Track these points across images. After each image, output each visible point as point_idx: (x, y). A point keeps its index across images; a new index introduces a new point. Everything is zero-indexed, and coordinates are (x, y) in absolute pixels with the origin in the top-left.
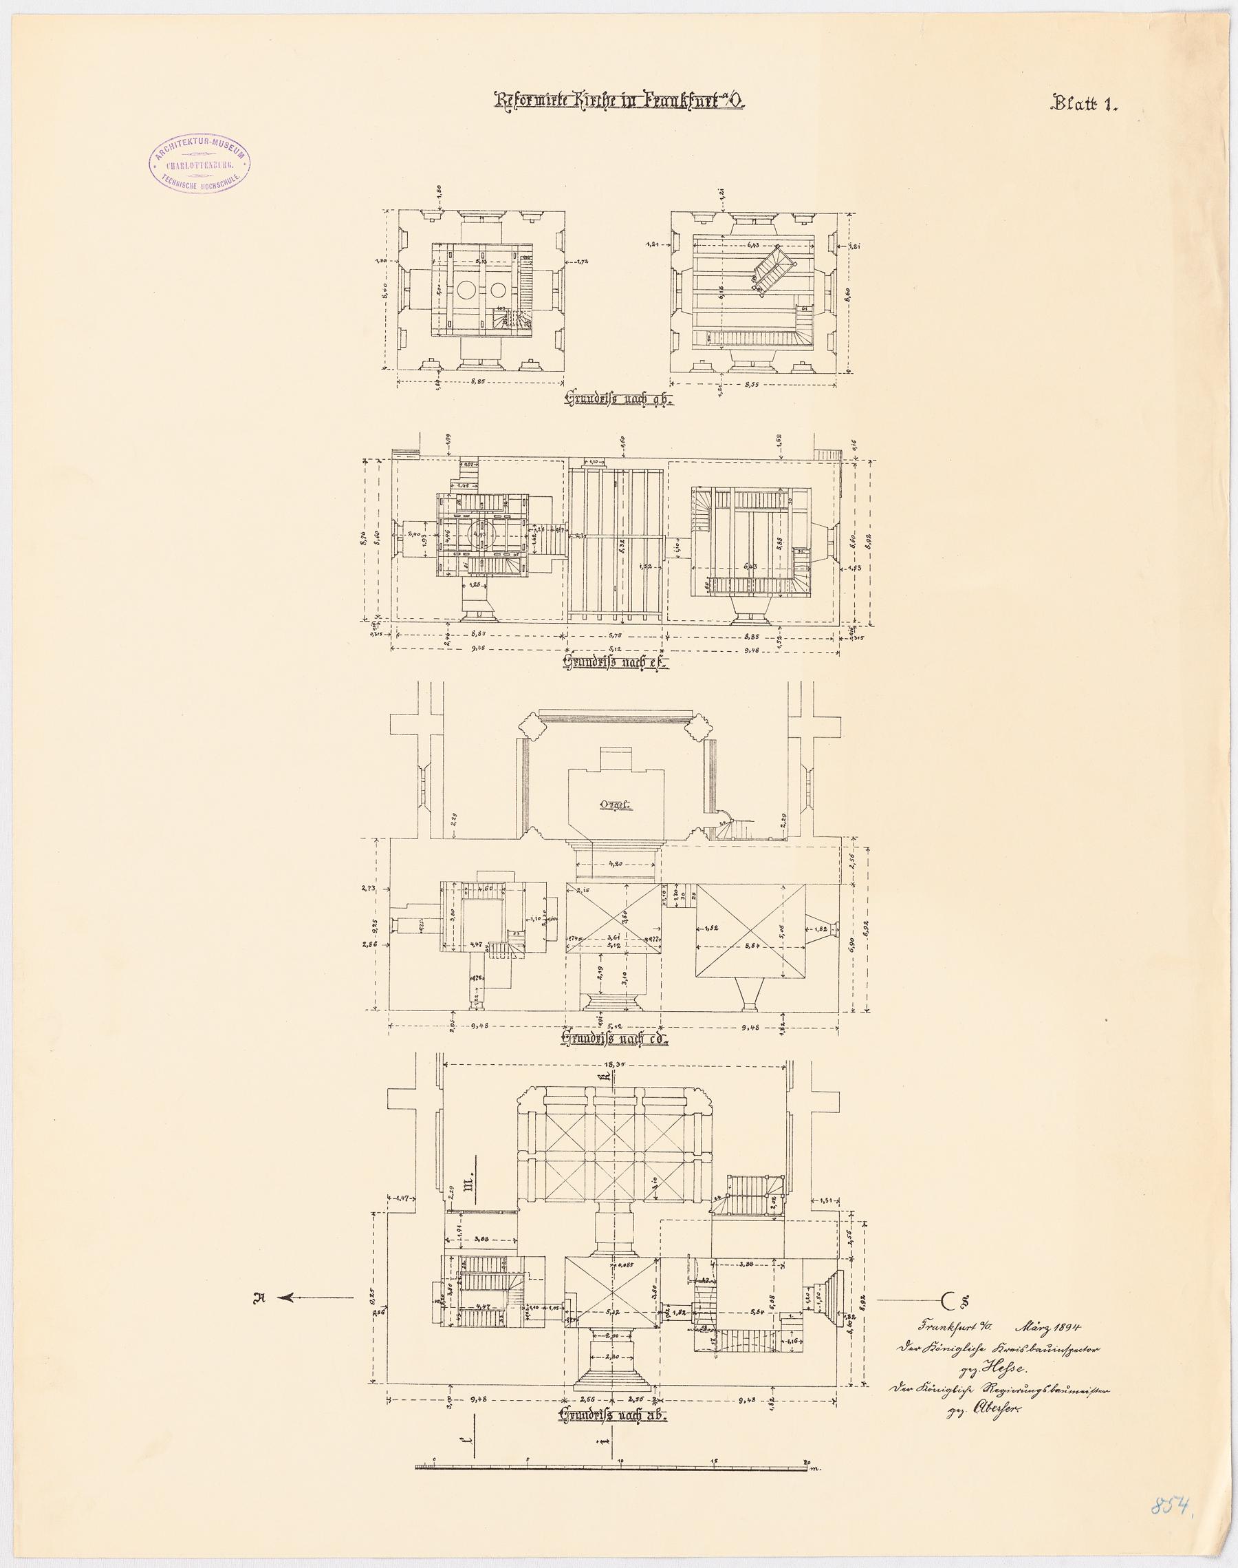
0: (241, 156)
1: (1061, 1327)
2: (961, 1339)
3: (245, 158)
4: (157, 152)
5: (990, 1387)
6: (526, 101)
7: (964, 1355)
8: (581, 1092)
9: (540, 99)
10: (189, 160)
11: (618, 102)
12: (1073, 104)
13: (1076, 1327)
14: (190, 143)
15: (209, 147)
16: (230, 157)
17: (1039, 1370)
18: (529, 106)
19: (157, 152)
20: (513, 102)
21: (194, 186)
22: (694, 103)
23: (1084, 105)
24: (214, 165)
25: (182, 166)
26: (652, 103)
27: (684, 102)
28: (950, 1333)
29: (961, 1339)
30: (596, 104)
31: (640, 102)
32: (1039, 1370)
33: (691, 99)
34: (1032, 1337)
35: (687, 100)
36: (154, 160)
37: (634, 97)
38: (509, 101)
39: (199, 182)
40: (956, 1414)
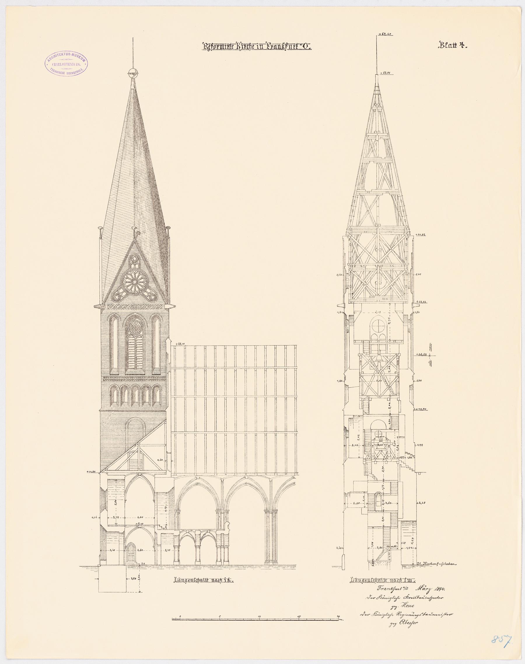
0: (84, 61)
1: (439, 589)
3: (86, 62)
8: (226, 559)
9: (222, 45)
10: (62, 62)
14: (62, 55)
15: (71, 57)
16: (80, 61)
18: (218, 49)
19: (48, 59)
20: (210, 47)
21: (64, 73)
22: (288, 47)
24: (73, 64)
25: (59, 64)
36: (47, 62)
38: (209, 47)
39: (66, 71)
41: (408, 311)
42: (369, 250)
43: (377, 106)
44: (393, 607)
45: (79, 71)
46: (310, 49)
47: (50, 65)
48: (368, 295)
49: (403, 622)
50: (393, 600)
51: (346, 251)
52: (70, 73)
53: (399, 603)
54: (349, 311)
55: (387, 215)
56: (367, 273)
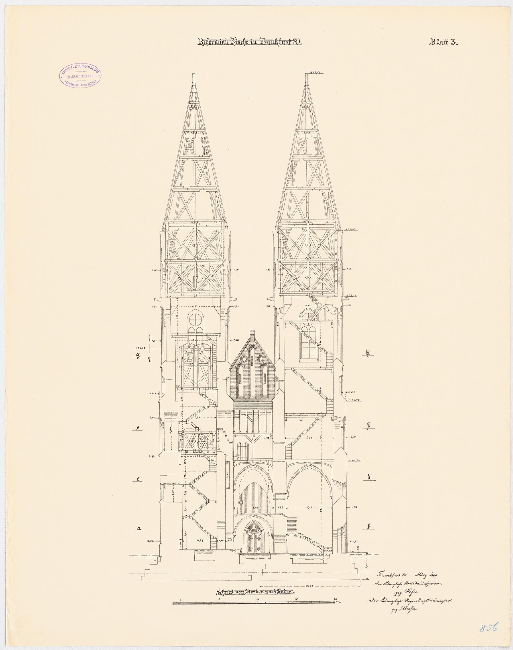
0: (97, 72)
1: (433, 575)
3: (99, 73)
4: (62, 72)
5: (407, 600)
6: (211, 42)
10: (76, 74)
11: (249, 42)
12: (439, 42)
14: (76, 67)
23: (443, 43)
24: (87, 76)
25: (73, 77)
27: (276, 43)
28: (390, 577)
30: (224, 43)
32: (422, 592)
33: (280, 41)
34: (419, 579)
37: (255, 40)
38: (202, 42)
39: (80, 83)
40: (394, 611)
41: (225, 306)
42: (299, 244)
43: (306, 104)
44: (396, 593)
48: (298, 289)
50: (396, 586)
51: (276, 246)
52: (84, 85)
54: (279, 303)
55: (317, 210)
56: (185, 267)
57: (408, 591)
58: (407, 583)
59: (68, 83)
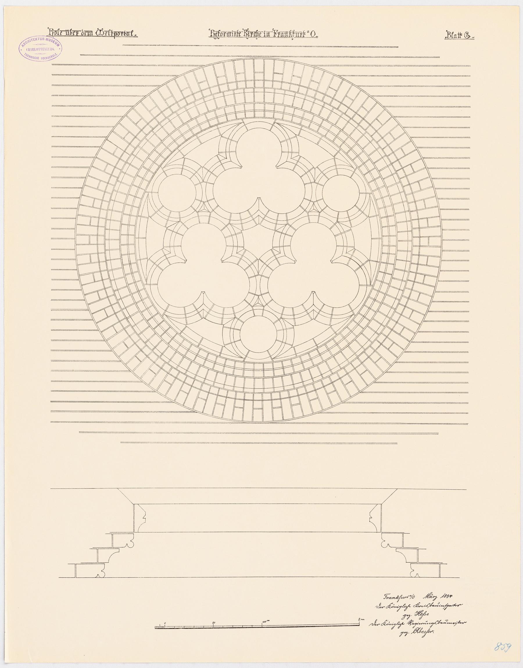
0: (58, 45)
1: (446, 596)
2: (401, 602)
3: (60, 46)
4: (22, 44)
6: (468, 96)
7: (402, 609)
10: (36, 47)
13: (451, 596)
14: (36, 39)
17: (434, 614)
21: (38, 58)
22: (295, 35)
25: (33, 49)
26: (277, 35)
28: (397, 600)
29: (401, 602)
31: (272, 34)
32: (434, 614)
34: (430, 601)
35: (292, 34)
36: (21, 47)
39: (40, 56)
45: (53, 56)
46: (317, 37)
47: (24, 51)
49: (417, 631)
52: (43, 58)
53: (409, 611)
57: (419, 613)
58: (417, 605)
59: (27, 56)
